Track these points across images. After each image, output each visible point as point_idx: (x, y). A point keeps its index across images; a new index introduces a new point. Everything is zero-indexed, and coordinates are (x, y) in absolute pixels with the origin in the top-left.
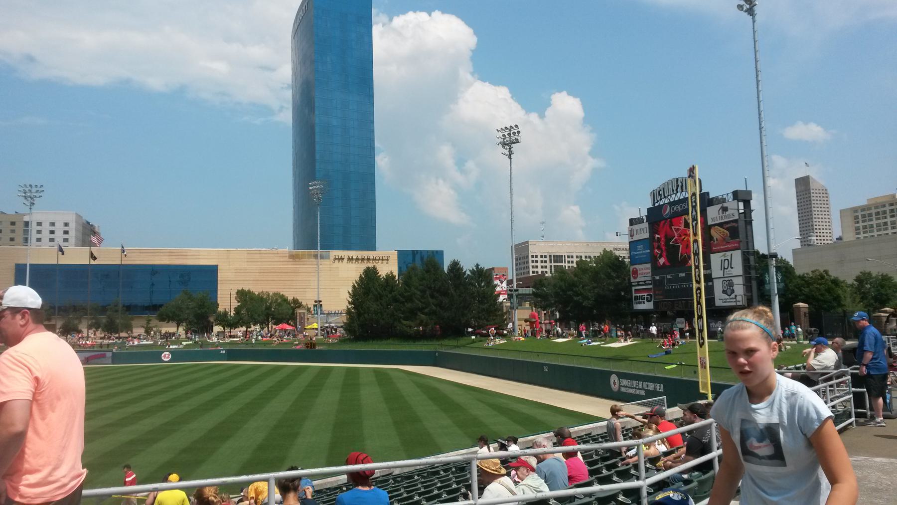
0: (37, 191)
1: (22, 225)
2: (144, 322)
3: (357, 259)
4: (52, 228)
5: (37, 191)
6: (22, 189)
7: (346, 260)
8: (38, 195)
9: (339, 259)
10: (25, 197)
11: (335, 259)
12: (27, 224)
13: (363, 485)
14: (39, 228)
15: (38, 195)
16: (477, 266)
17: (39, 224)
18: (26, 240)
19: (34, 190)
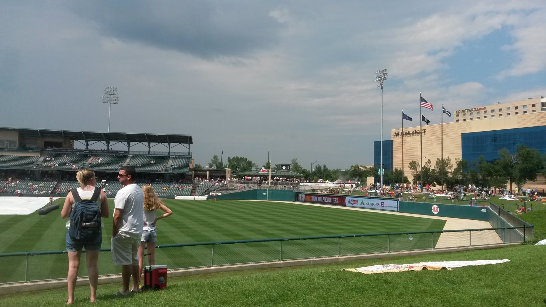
11: (425, 132)
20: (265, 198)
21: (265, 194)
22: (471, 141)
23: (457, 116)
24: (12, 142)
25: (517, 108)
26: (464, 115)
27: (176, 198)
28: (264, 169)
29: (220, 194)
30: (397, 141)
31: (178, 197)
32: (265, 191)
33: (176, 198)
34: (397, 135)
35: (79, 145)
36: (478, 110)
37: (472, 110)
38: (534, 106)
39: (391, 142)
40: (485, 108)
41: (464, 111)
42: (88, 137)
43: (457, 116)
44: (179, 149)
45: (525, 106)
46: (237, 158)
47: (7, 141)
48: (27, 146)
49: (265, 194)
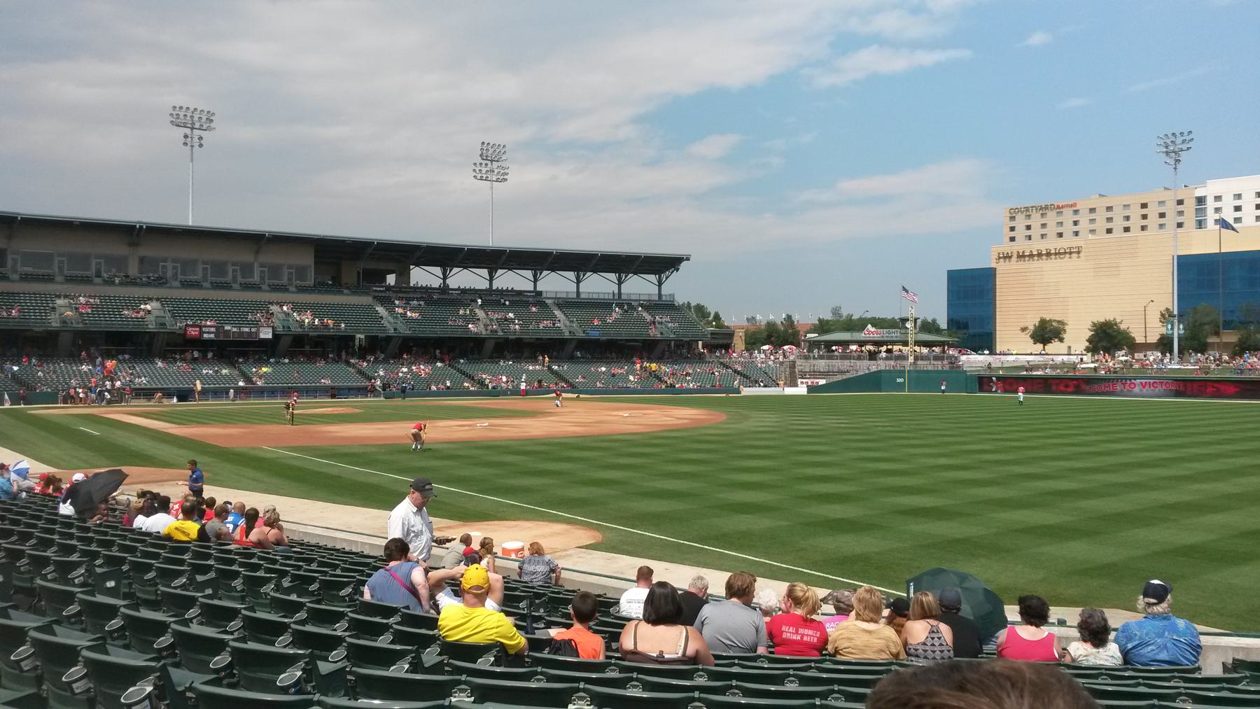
0: (1184, 141)
1: (1194, 202)
2: (583, 296)
3: (1031, 256)
4: (1238, 203)
5: (1184, 141)
6: (1161, 142)
7: (1014, 258)
8: (1184, 147)
9: (1005, 258)
10: (1167, 153)
11: (1079, 252)
12: (1201, 200)
13: (977, 349)
14: (1218, 204)
15: (1184, 147)
16: (789, 317)
17: (1218, 198)
18: (1200, 224)
19: (1179, 140)
20: (901, 387)
21: (899, 380)
22: (1196, 274)
23: (1012, 218)
24: (301, 272)
25: (1144, 206)
26: (1029, 216)
27: (743, 394)
28: (873, 329)
29: (822, 382)
30: (1002, 268)
31: (747, 391)
32: (901, 373)
33: (743, 394)
34: (1008, 257)
35: (423, 276)
36: (1058, 207)
37: (1046, 207)
38: (1180, 202)
39: (988, 276)
40: (1075, 205)
41: (1027, 209)
42: (447, 257)
43: (1012, 218)
44: (639, 286)
45: (1161, 203)
46: (700, 310)
47: (290, 267)
48: (344, 281)
49: (899, 380)
